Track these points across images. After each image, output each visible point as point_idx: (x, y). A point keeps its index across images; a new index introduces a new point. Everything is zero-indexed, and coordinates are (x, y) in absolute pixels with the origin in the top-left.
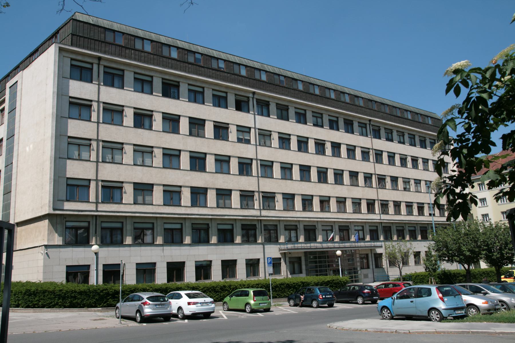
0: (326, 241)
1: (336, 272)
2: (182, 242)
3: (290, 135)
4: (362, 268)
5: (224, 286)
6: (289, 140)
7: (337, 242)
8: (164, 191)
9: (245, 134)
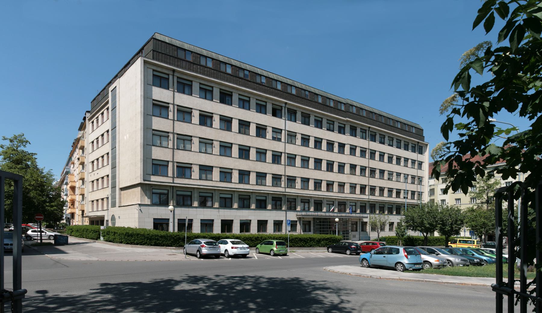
0: (328, 211)
1: (334, 232)
2: (232, 207)
3: (309, 136)
4: (352, 231)
5: (258, 237)
6: (309, 139)
7: (336, 213)
8: (220, 172)
9: (278, 134)
